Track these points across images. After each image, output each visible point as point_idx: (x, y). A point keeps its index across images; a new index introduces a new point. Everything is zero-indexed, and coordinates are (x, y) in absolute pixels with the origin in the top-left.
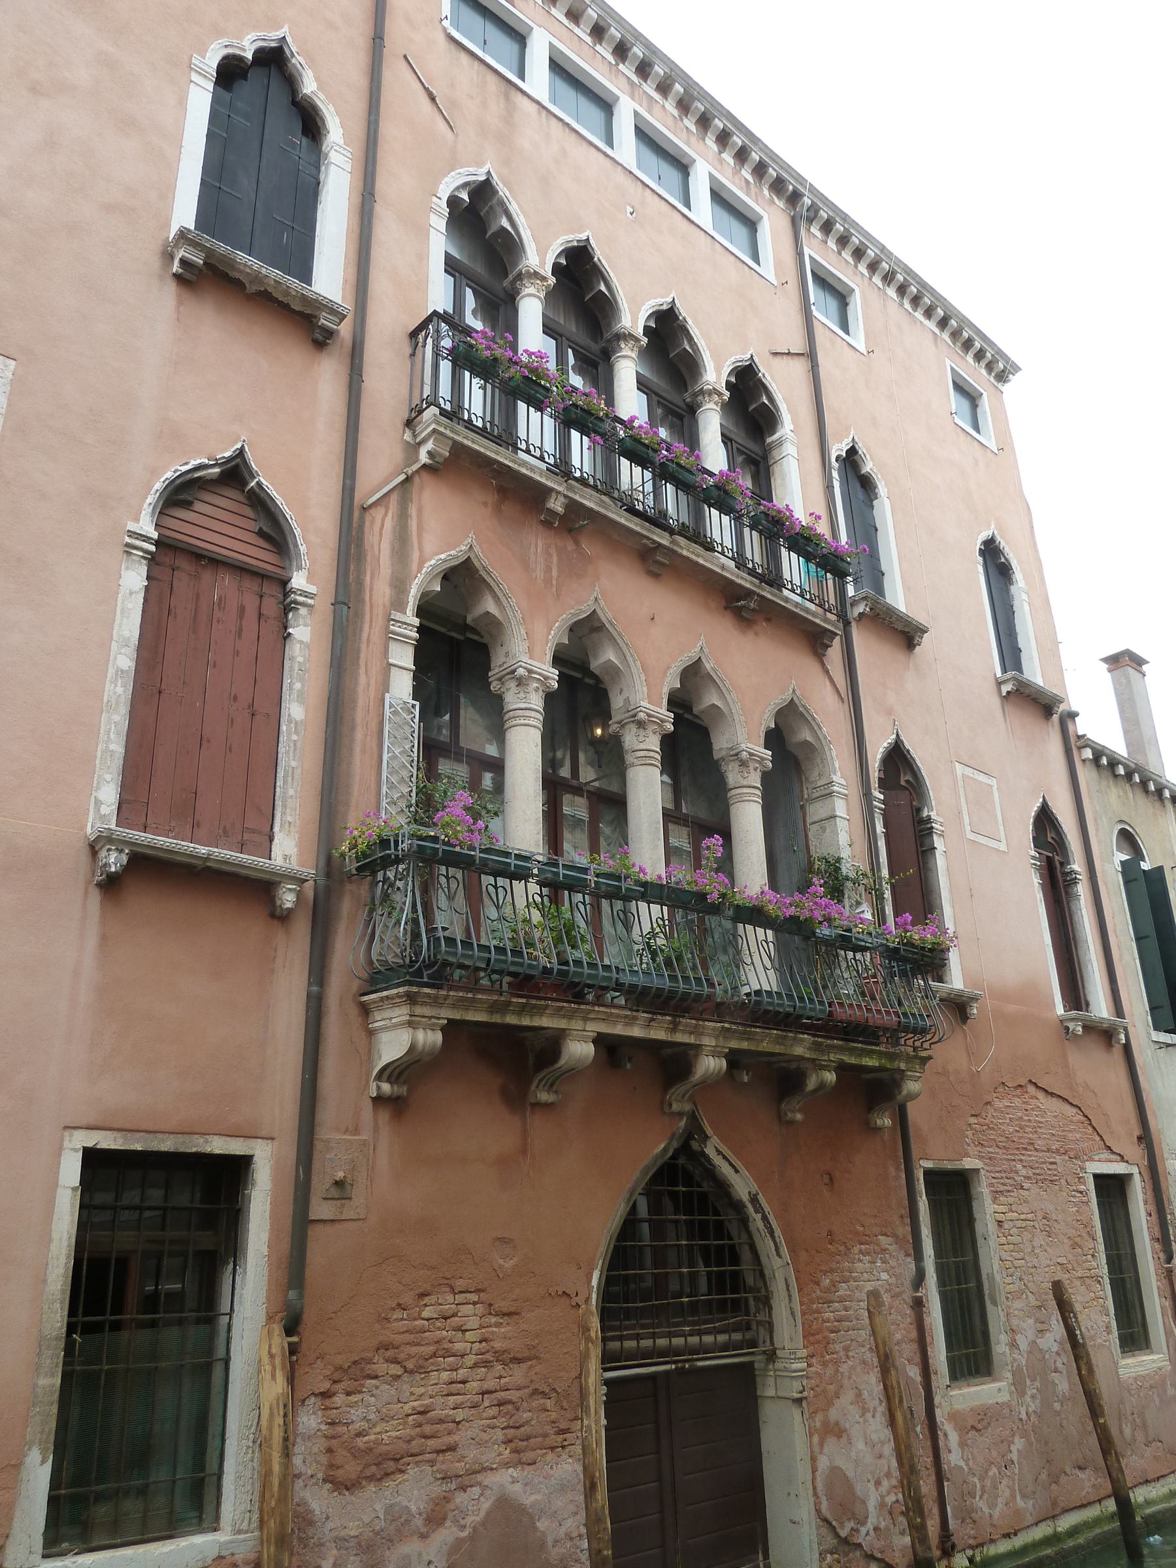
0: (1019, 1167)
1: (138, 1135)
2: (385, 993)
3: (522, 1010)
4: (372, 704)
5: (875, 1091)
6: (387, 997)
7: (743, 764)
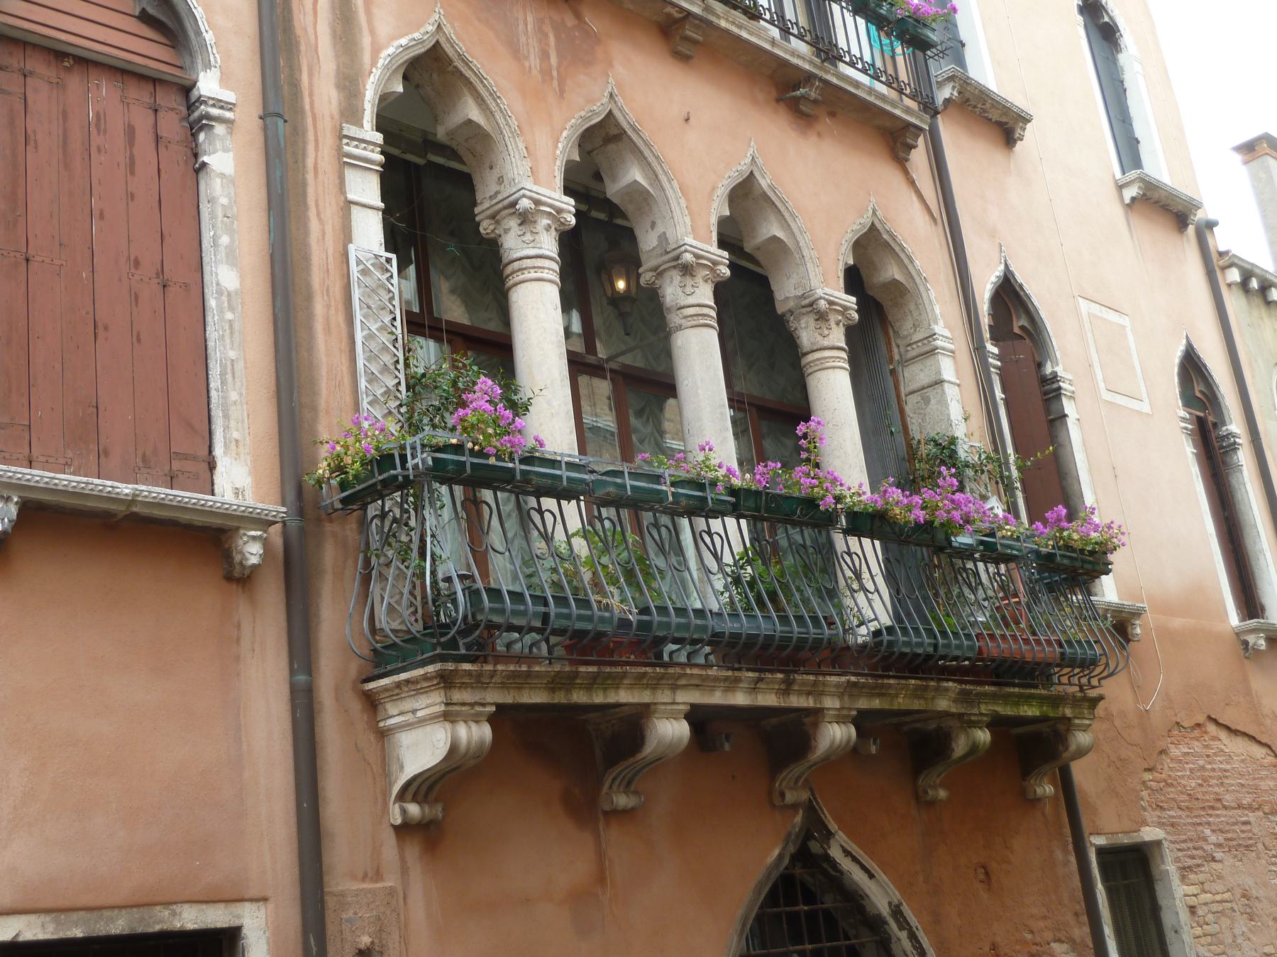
0: (1208, 832)
1: (75, 916)
2: (404, 676)
3: (593, 683)
4: (331, 260)
5: (1035, 749)
6: (408, 681)
7: (822, 317)
